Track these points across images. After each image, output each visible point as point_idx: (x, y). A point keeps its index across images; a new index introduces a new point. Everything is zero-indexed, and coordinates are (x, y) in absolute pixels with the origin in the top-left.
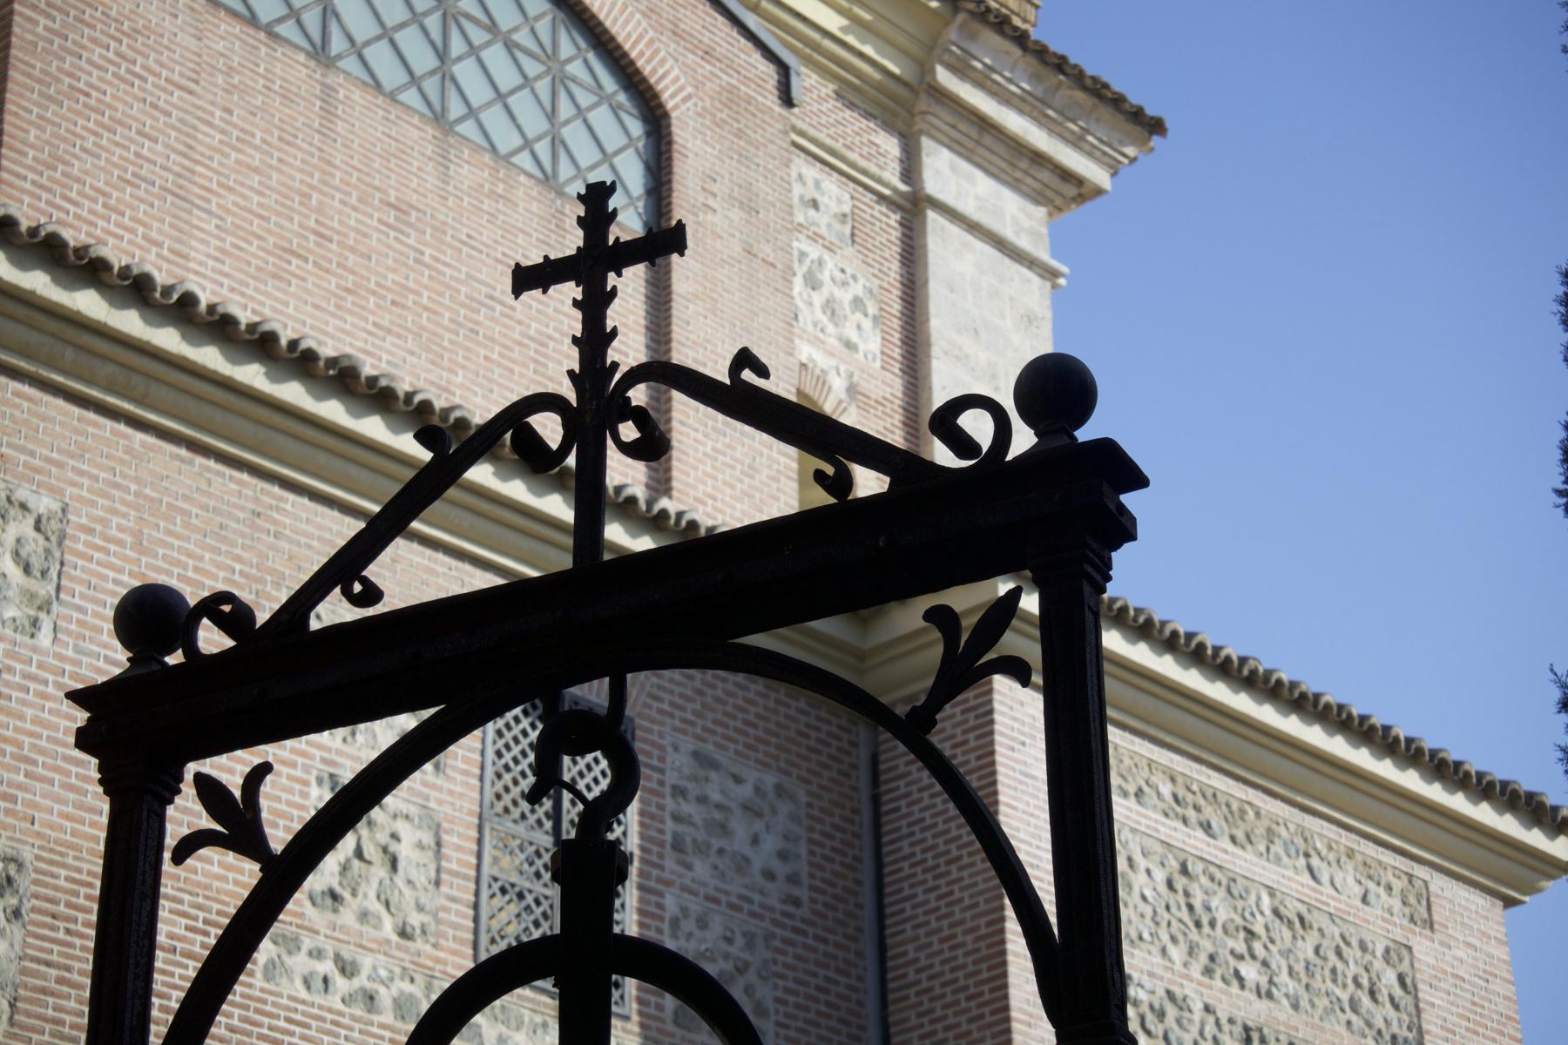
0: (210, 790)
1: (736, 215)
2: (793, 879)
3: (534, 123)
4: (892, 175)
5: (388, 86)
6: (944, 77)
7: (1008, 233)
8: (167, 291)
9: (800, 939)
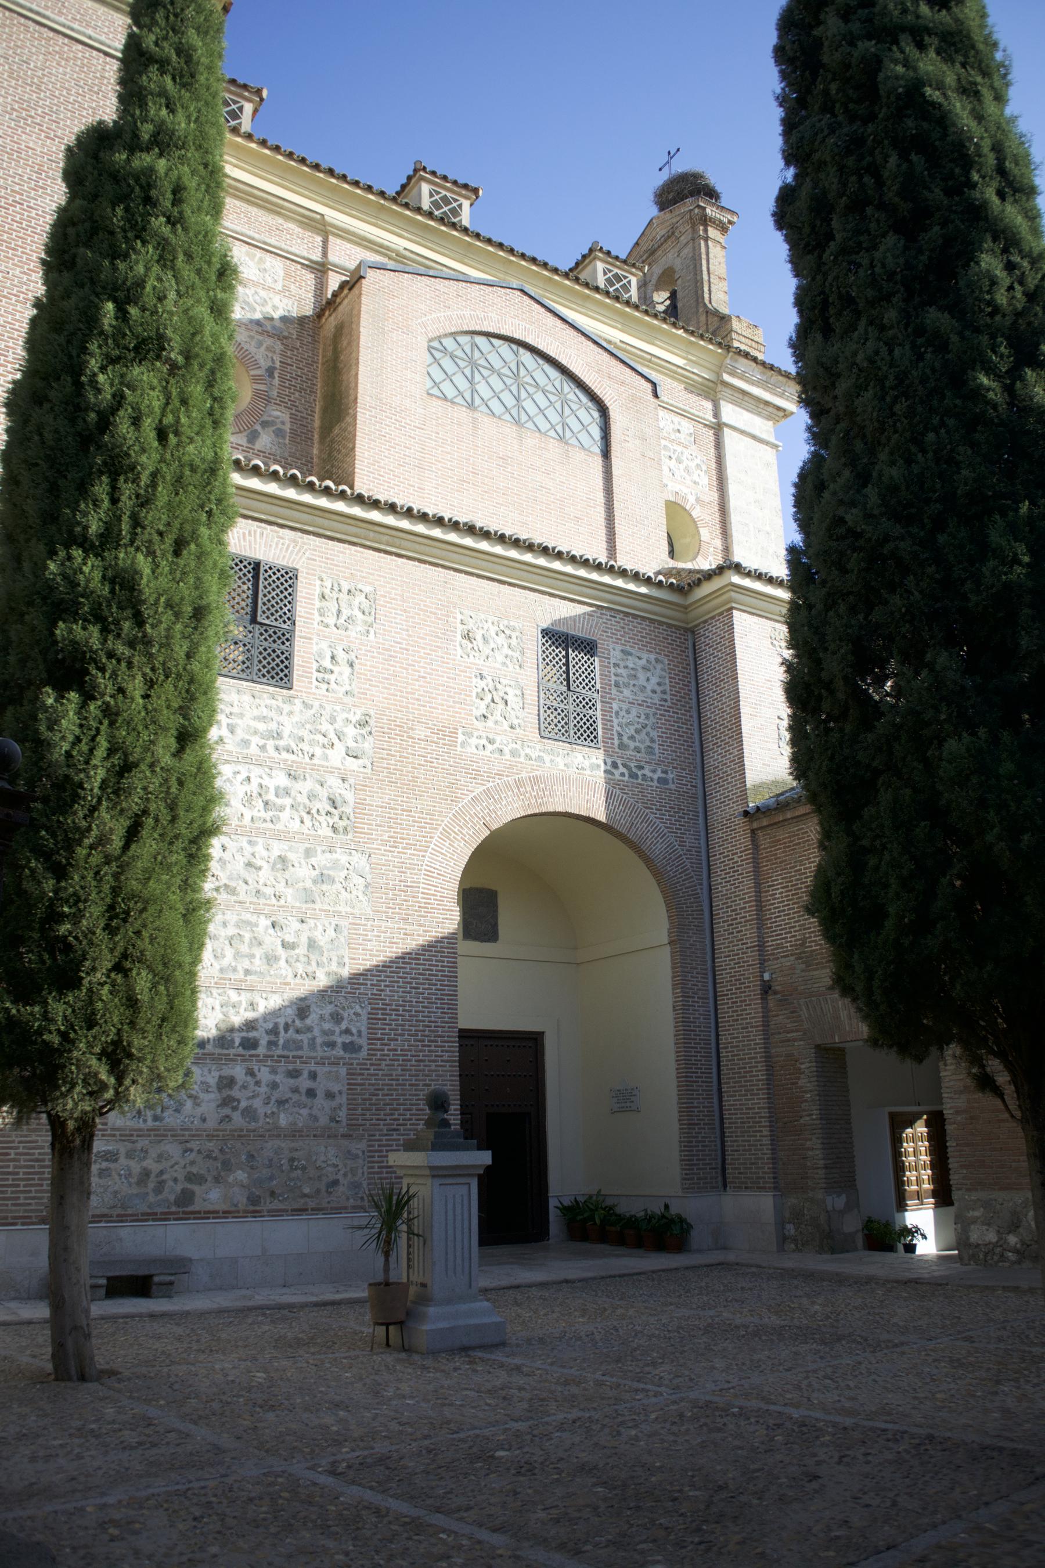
1: (638, 442)
2: (664, 692)
3: (555, 418)
5: (497, 414)
6: (726, 377)
8: (402, 507)
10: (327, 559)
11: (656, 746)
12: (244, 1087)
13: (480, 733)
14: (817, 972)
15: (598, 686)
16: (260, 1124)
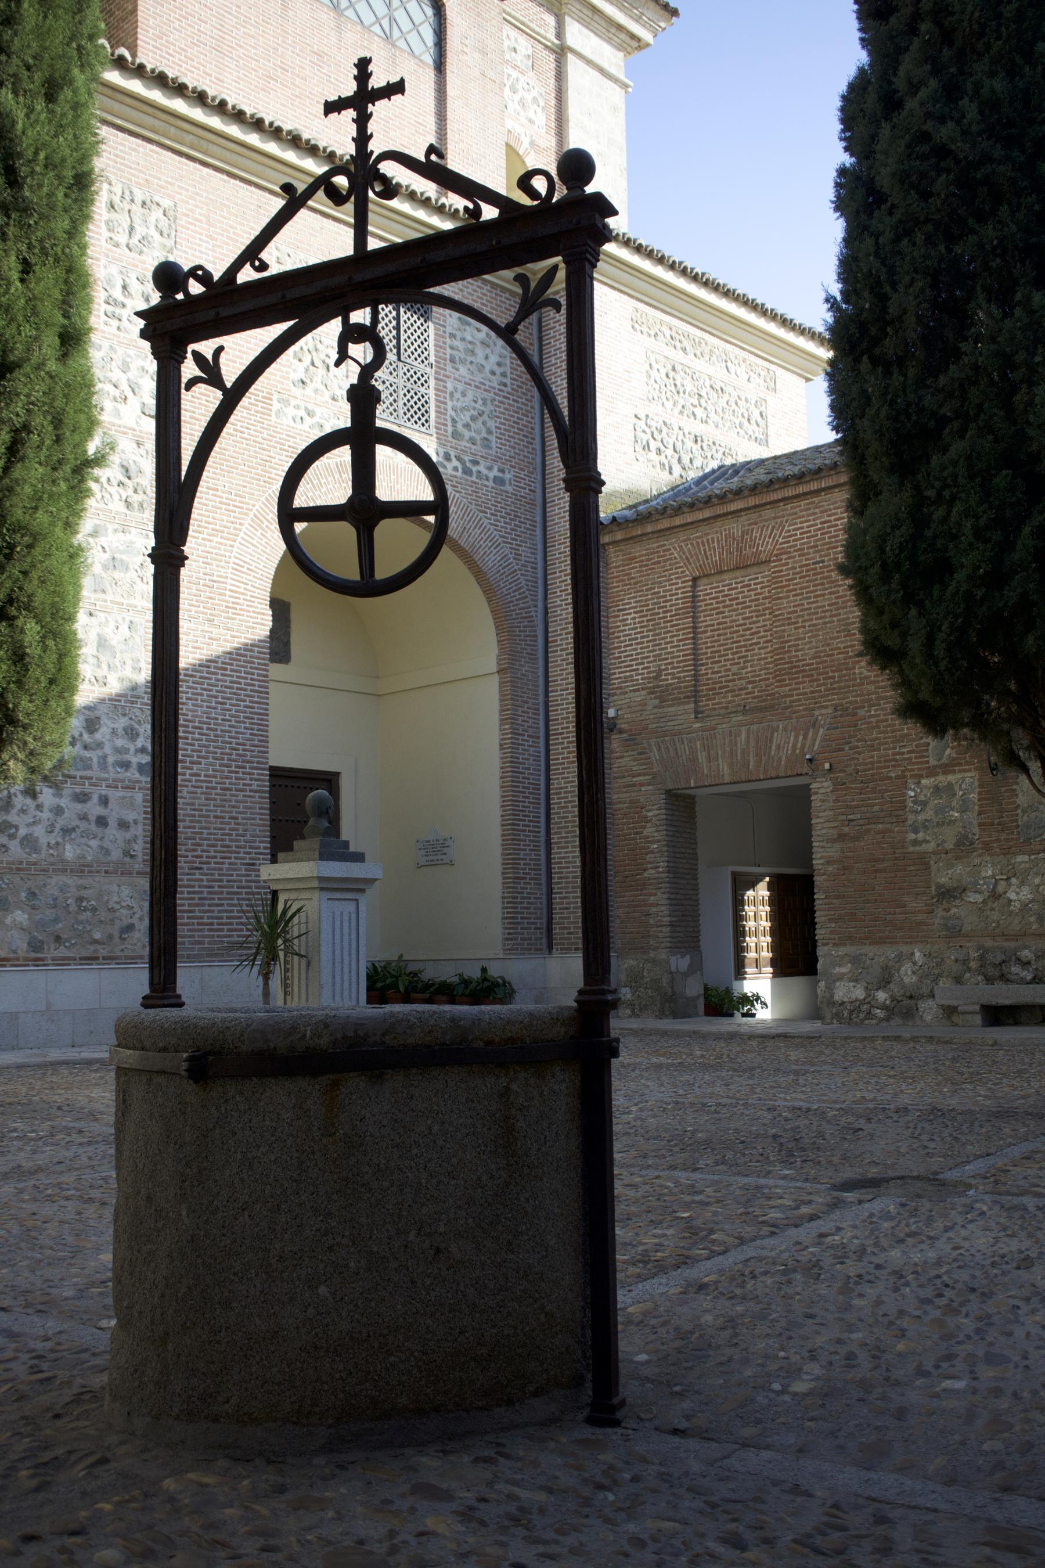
0: (198, 357)
1: (477, 55)
2: (504, 375)
4: (551, 35)
7: (605, 65)
8: (213, 99)
9: (506, 401)
10: (116, 156)
11: (493, 439)
12: (23, 811)
13: (298, 402)
14: (673, 709)
15: (432, 359)
16: (43, 856)
